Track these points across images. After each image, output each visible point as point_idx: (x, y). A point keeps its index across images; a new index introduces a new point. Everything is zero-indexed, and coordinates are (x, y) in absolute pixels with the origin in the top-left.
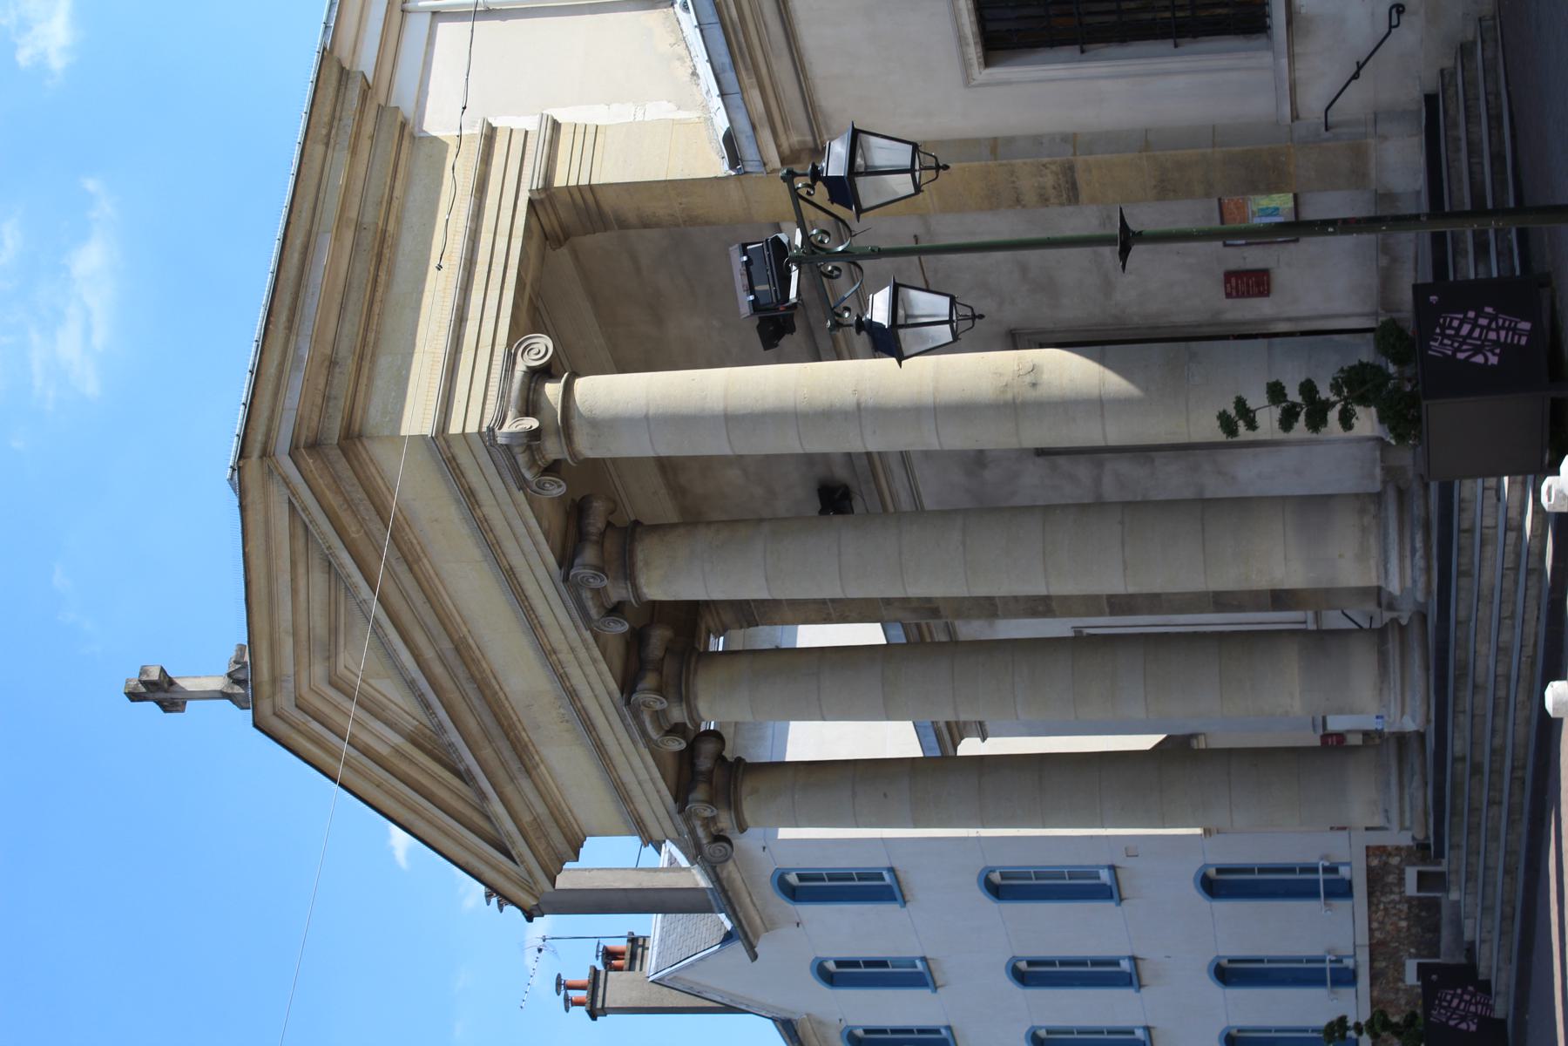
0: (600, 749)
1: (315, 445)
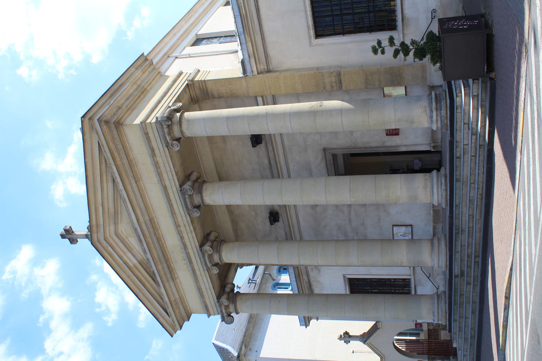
0: (194, 271)
1: (107, 122)
